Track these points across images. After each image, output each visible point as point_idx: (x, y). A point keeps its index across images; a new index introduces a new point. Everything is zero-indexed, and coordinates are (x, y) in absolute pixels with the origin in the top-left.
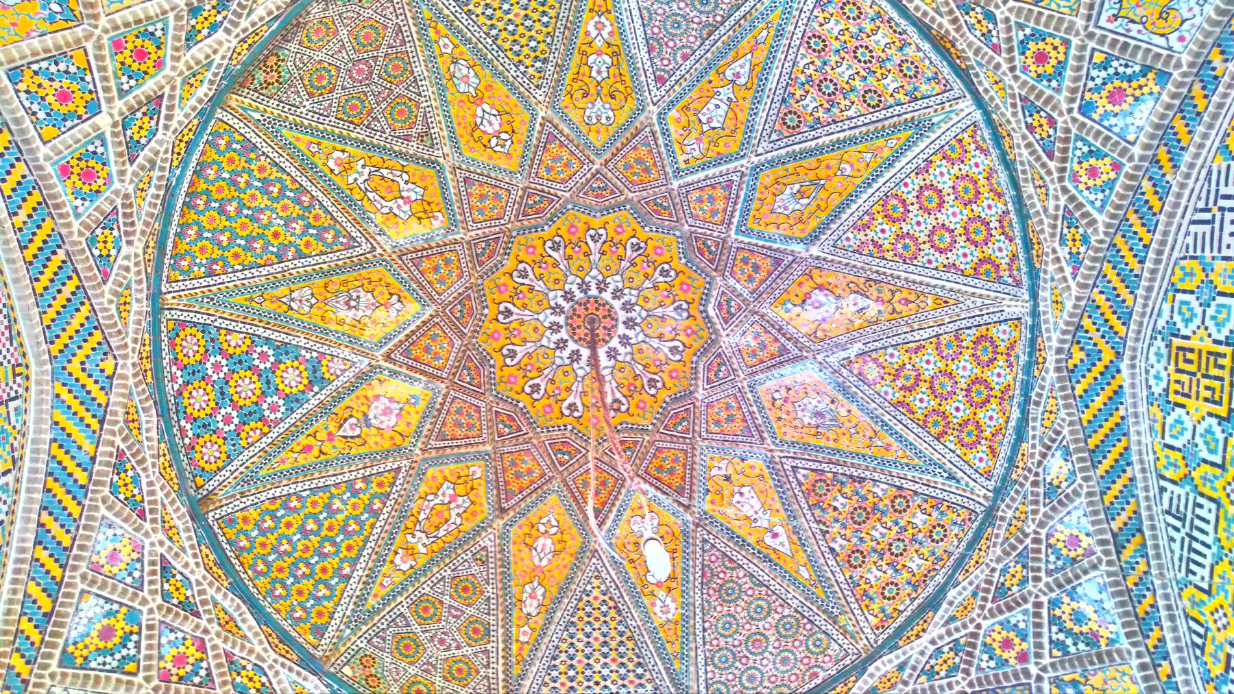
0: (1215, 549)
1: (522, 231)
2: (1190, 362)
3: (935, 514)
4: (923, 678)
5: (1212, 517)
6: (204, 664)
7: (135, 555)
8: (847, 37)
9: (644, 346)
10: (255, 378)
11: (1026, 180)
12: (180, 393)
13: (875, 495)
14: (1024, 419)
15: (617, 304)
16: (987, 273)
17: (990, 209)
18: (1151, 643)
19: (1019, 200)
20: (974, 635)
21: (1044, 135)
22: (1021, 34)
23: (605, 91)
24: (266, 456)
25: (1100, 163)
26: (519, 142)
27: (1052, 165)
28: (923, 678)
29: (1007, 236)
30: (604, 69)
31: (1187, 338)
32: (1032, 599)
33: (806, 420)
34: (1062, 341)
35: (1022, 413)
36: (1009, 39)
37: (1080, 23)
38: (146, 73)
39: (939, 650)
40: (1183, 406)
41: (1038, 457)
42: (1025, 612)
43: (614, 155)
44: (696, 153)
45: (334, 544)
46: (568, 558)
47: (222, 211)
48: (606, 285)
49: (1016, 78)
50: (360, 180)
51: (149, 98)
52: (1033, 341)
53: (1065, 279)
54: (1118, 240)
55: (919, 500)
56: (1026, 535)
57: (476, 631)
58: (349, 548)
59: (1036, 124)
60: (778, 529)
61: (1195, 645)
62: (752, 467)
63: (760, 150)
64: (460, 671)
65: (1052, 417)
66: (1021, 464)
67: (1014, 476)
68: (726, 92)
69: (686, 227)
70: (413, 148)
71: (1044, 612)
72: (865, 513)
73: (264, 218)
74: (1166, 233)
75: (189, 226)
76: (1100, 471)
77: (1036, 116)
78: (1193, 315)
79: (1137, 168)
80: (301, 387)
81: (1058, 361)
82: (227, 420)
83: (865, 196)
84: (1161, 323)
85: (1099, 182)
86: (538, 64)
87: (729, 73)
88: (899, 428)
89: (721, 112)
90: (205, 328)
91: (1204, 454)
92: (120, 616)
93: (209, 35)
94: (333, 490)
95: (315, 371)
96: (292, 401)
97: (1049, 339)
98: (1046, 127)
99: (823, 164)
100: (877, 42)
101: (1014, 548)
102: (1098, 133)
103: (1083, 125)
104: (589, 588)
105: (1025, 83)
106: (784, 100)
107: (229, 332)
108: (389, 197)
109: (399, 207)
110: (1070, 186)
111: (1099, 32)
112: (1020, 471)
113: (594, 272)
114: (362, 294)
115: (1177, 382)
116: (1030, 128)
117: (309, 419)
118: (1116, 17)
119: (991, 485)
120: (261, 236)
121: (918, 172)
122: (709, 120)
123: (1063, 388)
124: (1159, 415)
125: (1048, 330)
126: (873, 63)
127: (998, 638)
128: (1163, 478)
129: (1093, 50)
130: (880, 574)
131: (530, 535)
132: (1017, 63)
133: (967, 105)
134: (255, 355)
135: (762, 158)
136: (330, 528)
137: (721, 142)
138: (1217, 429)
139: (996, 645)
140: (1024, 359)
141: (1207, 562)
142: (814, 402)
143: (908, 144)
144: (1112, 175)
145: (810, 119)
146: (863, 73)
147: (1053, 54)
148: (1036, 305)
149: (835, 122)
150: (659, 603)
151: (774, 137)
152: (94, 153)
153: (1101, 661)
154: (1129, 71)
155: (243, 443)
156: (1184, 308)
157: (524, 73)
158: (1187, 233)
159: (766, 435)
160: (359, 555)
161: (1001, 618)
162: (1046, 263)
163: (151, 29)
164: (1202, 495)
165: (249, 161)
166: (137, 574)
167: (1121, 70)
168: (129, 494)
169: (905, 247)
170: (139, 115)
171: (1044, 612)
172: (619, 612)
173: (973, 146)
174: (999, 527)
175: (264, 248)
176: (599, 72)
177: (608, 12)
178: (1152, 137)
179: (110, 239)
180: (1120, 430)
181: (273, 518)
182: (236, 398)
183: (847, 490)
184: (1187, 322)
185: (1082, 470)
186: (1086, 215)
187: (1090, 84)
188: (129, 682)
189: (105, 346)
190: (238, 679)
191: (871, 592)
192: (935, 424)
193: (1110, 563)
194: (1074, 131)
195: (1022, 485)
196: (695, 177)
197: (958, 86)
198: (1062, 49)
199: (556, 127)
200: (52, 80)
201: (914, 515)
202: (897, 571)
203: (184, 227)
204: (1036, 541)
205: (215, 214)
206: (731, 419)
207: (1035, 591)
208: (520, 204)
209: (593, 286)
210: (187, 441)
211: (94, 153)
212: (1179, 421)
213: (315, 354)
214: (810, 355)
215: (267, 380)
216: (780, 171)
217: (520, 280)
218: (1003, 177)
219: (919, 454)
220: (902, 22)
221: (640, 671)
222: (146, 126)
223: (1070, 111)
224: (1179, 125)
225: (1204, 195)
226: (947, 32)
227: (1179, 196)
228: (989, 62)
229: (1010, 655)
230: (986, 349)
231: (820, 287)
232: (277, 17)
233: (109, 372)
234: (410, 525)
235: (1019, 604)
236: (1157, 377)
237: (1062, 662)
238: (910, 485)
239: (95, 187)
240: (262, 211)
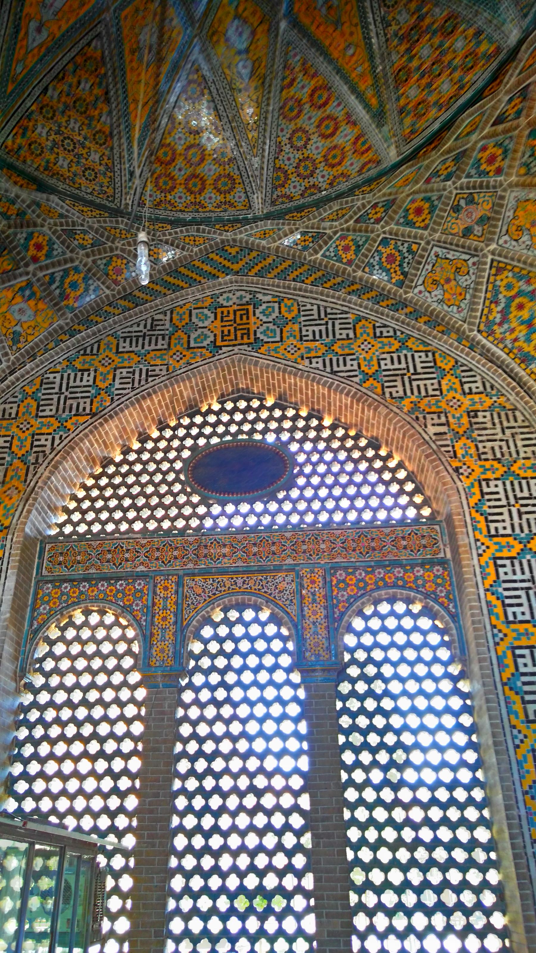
0: (143, 351)
2: (241, 319)
3: (102, 168)
5: (159, 347)
11: (341, 204)
14: (185, 223)
16: (278, 178)
17: (322, 177)
18: (76, 327)
19: (328, 200)
20: (35, 225)
25: (352, 252)
31: (254, 315)
32: (74, 255)
34: (241, 242)
35: (190, 221)
37: (437, 236)
40: (216, 318)
42: (64, 253)
52: (237, 221)
54: (306, 267)
55: (107, 153)
56: (113, 242)
59: (378, 209)
61: (85, 349)
65: (192, 243)
71: (69, 265)
74: (311, 292)
76: (166, 278)
78: (267, 316)
79: (349, 275)
84: (260, 296)
85: (341, 252)
91: (193, 336)
97: (241, 233)
98: (375, 217)
99: (353, 29)
102: (369, 251)
103: (375, 241)
111: (430, 247)
115: (229, 312)
116: (375, 206)
118: (437, 256)
121: (348, 116)
124: (207, 304)
125: (246, 230)
128: (172, 313)
129: (420, 244)
138: (208, 341)
140: (226, 216)
141: (134, 348)
143: (367, 106)
144: (345, 261)
145: (390, 18)
147: (420, 219)
153: (55, 305)
154: (405, 265)
156: (270, 310)
158: (312, 304)
161: (54, 238)
162: (289, 224)
164: (170, 338)
167: (406, 260)
171: (69, 265)
174: (111, 222)
178: (367, 282)
180: (192, 282)
183: (97, 91)
184: (263, 312)
186: (321, 248)
187: (399, 243)
191: (29, 133)
193: (114, 296)
194: (372, 235)
197: (407, 150)
198: (422, 225)
201: (96, 151)
202: (52, 149)
212: (207, 317)
218: (344, 186)
224: (373, 294)
225: (334, 311)
227: (333, 297)
229: (32, 251)
230: (226, 184)
231: (253, 33)
235: (68, 248)
236: (228, 299)
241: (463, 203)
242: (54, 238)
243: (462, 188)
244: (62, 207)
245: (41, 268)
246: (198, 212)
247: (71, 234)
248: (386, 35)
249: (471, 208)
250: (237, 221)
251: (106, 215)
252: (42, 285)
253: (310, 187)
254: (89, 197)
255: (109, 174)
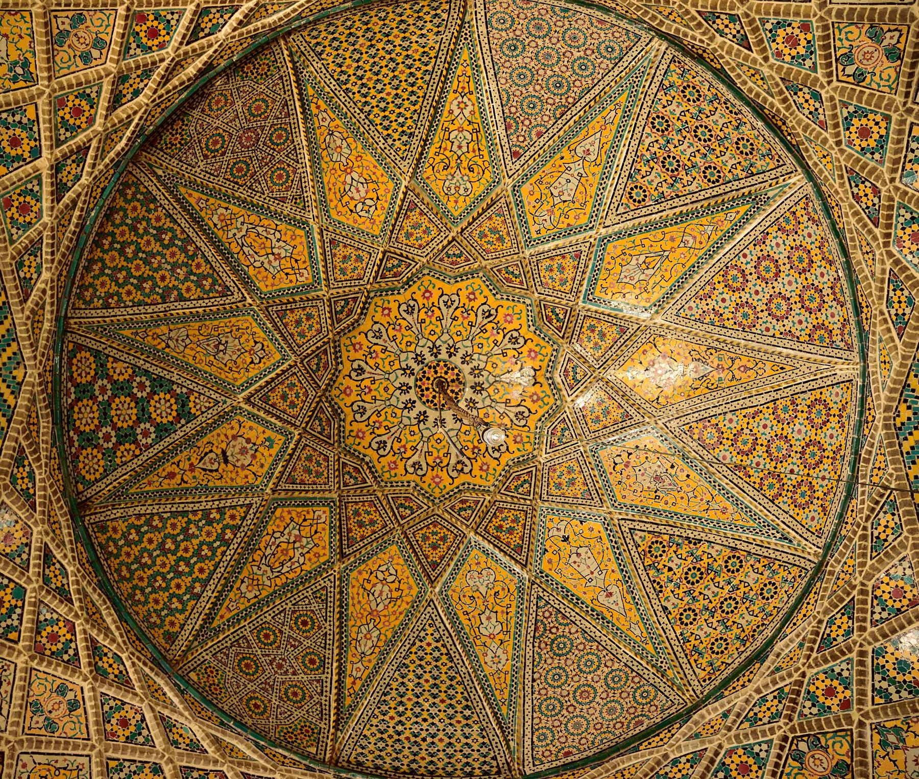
1: (381, 292)
3: (766, 573)
4: (746, 725)
6: (73, 645)
7: (24, 540)
8: (688, 118)
9: (490, 411)
10: (133, 404)
12: (72, 407)
13: (710, 556)
15: (466, 369)
16: (821, 339)
19: (849, 266)
20: (800, 684)
21: (870, 204)
22: (845, 111)
23: (465, 164)
24: (137, 477)
26: (383, 208)
27: (877, 231)
28: (746, 725)
29: (839, 302)
30: (464, 144)
32: (857, 648)
33: (646, 484)
34: (891, 399)
35: (853, 471)
36: (835, 116)
37: (899, 99)
38: (79, 127)
39: (764, 699)
41: (866, 512)
43: (470, 224)
44: (548, 225)
45: (188, 564)
46: (404, 606)
47: (122, 252)
48: (456, 350)
49: (842, 151)
50: (239, 235)
51: (79, 147)
52: (863, 401)
53: (893, 340)
57: (312, 662)
58: (201, 570)
59: (861, 194)
60: (613, 589)
62: (591, 529)
63: (608, 223)
64: (295, 694)
65: (881, 473)
66: (850, 520)
67: (844, 532)
68: (576, 168)
69: (536, 295)
70: (287, 209)
72: (698, 573)
73: (155, 263)
75: (95, 262)
77: (862, 186)
80: (170, 418)
81: (885, 419)
82: (107, 438)
83: (706, 267)
86: (405, 138)
87: (580, 151)
88: (735, 491)
89: (572, 186)
90: (96, 354)
92: (8, 591)
93: (132, 99)
94: (190, 516)
95: (183, 406)
96: (163, 431)
97: (878, 398)
98: (871, 196)
99: (668, 237)
100: (716, 122)
101: (842, 600)
103: (906, 193)
104: (422, 634)
105: (850, 156)
106: (630, 176)
107: (116, 360)
108: (263, 252)
109: (270, 262)
110: (894, 249)
112: (849, 527)
113: (445, 337)
114: (230, 340)
116: (857, 198)
117: (175, 449)
119: (821, 542)
120: (151, 278)
122: (561, 193)
123: (891, 445)
125: (877, 389)
126: (709, 140)
127: (822, 686)
129: (912, 123)
130: (710, 630)
131: (369, 581)
132: (842, 137)
133: (798, 178)
134: (135, 384)
135: (610, 230)
136: (186, 550)
137: (572, 214)
139: (819, 693)
142: (655, 467)
143: (746, 219)
146: (703, 151)
147: (875, 129)
148: (865, 368)
149: (678, 196)
150: (490, 654)
151: (621, 210)
152: (32, 190)
155: (118, 461)
157: (391, 146)
159: (605, 498)
160: (210, 577)
161: (825, 667)
162: (875, 325)
163: (88, 91)
165: (149, 211)
166: (25, 556)
168: (24, 487)
169: (745, 316)
170: (69, 162)
172: (451, 659)
173: (806, 218)
174: (828, 581)
175: (152, 289)
176: (460, 147)
177: (471, 93)
179: (34, 264)
181: (138, 532)
182: (115, 419)
183: (683, 552)
185: (909, 522)
188: (10, 648)
189: (19, 356)
190: (100, 664)
192: (771, 486)
194: (897, 199)
195: (851, 540)
196: (547, 247)
197: (790, 160)
198: (883, 124)
199: (417, 196)
200: (8, 128)
203: (91, 262)
204: (863, 592)
205: (116, 254)
206: (572, 482)
207: (860, 640)
208: (379, 267)
209: (444, 350)
210: (73, 450)
211: (32, 190)
213: (184, 390)
214: (652, 421)
215: (142, 406)
216: (626, 242)
217: (374, 341)
218: (833, 245)
219: (754, 516)
220: (738, 103)
221: (467, 713)
222: (73, 172)
223: (892, 180)
226: (778, 110)
228: (817, 137)
229: (833, 702)
232: (188, 87)
233: (19, 379)
234: (257, 558)
235: (843, 654)
237: (884, 709)
238: (744, 546)
239: (28, 219)
240: (153, 256)
241: (850, 70)
242: (825, 667)
243: (830, 74)
244: (791, 641)
245: (861, 702)
246: (843, 457)
247: (827, 641)
248: (672, 198)
249: (858, 55)
250: (863, 401)
251: (818, 585)
252: (886, 714)
253: (834, 293)
254: (792, 601)
255: (776, 567)
